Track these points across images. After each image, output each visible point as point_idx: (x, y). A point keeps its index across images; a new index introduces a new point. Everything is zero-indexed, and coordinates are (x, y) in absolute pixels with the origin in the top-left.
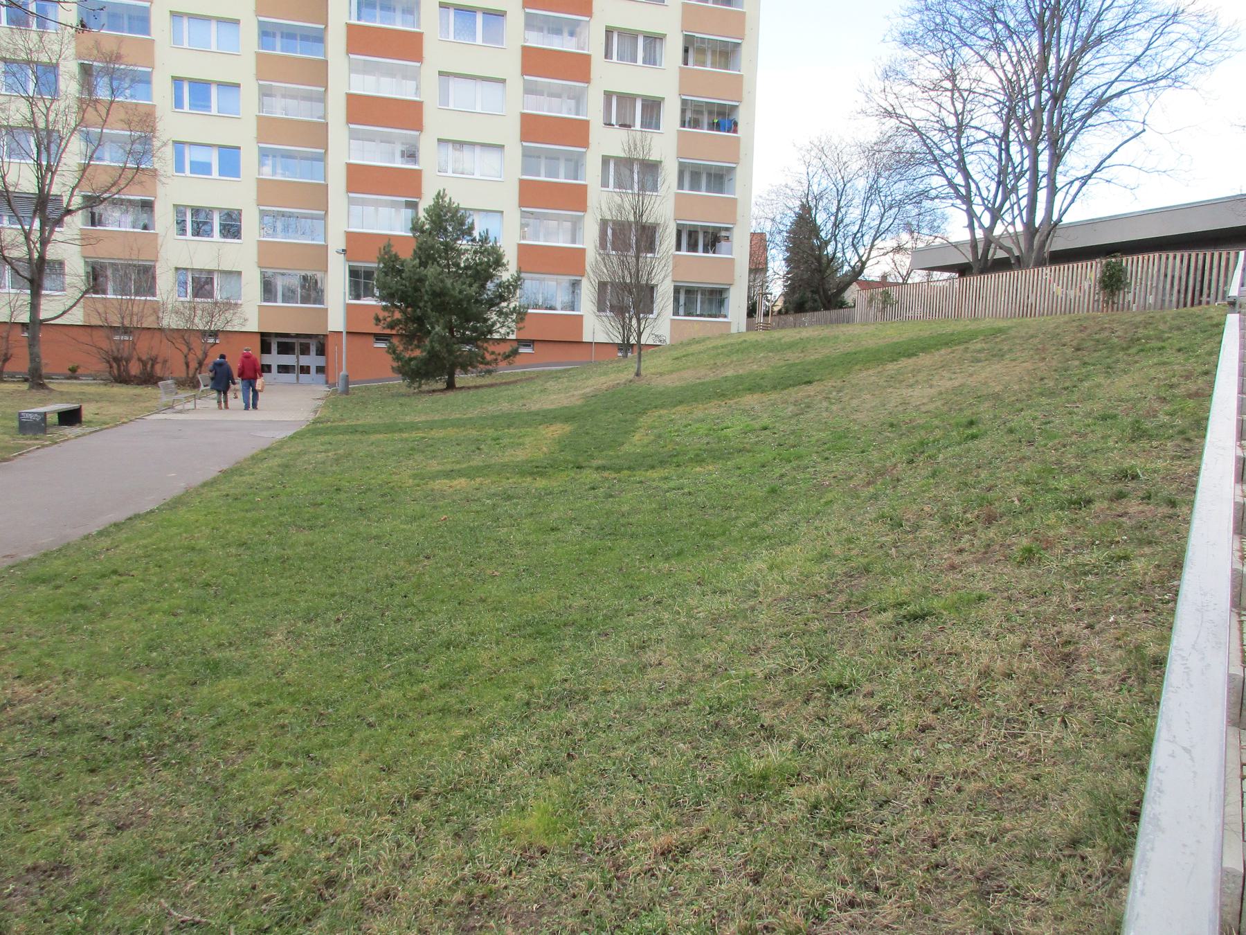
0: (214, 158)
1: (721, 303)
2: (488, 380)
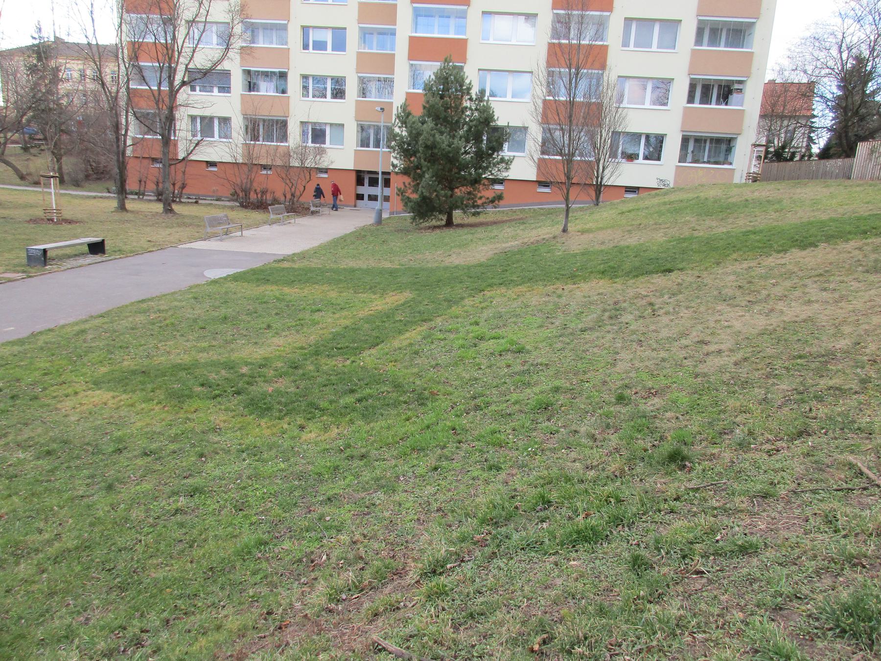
0: (328, 37)
1: (729, 150)
2: (473, 220)
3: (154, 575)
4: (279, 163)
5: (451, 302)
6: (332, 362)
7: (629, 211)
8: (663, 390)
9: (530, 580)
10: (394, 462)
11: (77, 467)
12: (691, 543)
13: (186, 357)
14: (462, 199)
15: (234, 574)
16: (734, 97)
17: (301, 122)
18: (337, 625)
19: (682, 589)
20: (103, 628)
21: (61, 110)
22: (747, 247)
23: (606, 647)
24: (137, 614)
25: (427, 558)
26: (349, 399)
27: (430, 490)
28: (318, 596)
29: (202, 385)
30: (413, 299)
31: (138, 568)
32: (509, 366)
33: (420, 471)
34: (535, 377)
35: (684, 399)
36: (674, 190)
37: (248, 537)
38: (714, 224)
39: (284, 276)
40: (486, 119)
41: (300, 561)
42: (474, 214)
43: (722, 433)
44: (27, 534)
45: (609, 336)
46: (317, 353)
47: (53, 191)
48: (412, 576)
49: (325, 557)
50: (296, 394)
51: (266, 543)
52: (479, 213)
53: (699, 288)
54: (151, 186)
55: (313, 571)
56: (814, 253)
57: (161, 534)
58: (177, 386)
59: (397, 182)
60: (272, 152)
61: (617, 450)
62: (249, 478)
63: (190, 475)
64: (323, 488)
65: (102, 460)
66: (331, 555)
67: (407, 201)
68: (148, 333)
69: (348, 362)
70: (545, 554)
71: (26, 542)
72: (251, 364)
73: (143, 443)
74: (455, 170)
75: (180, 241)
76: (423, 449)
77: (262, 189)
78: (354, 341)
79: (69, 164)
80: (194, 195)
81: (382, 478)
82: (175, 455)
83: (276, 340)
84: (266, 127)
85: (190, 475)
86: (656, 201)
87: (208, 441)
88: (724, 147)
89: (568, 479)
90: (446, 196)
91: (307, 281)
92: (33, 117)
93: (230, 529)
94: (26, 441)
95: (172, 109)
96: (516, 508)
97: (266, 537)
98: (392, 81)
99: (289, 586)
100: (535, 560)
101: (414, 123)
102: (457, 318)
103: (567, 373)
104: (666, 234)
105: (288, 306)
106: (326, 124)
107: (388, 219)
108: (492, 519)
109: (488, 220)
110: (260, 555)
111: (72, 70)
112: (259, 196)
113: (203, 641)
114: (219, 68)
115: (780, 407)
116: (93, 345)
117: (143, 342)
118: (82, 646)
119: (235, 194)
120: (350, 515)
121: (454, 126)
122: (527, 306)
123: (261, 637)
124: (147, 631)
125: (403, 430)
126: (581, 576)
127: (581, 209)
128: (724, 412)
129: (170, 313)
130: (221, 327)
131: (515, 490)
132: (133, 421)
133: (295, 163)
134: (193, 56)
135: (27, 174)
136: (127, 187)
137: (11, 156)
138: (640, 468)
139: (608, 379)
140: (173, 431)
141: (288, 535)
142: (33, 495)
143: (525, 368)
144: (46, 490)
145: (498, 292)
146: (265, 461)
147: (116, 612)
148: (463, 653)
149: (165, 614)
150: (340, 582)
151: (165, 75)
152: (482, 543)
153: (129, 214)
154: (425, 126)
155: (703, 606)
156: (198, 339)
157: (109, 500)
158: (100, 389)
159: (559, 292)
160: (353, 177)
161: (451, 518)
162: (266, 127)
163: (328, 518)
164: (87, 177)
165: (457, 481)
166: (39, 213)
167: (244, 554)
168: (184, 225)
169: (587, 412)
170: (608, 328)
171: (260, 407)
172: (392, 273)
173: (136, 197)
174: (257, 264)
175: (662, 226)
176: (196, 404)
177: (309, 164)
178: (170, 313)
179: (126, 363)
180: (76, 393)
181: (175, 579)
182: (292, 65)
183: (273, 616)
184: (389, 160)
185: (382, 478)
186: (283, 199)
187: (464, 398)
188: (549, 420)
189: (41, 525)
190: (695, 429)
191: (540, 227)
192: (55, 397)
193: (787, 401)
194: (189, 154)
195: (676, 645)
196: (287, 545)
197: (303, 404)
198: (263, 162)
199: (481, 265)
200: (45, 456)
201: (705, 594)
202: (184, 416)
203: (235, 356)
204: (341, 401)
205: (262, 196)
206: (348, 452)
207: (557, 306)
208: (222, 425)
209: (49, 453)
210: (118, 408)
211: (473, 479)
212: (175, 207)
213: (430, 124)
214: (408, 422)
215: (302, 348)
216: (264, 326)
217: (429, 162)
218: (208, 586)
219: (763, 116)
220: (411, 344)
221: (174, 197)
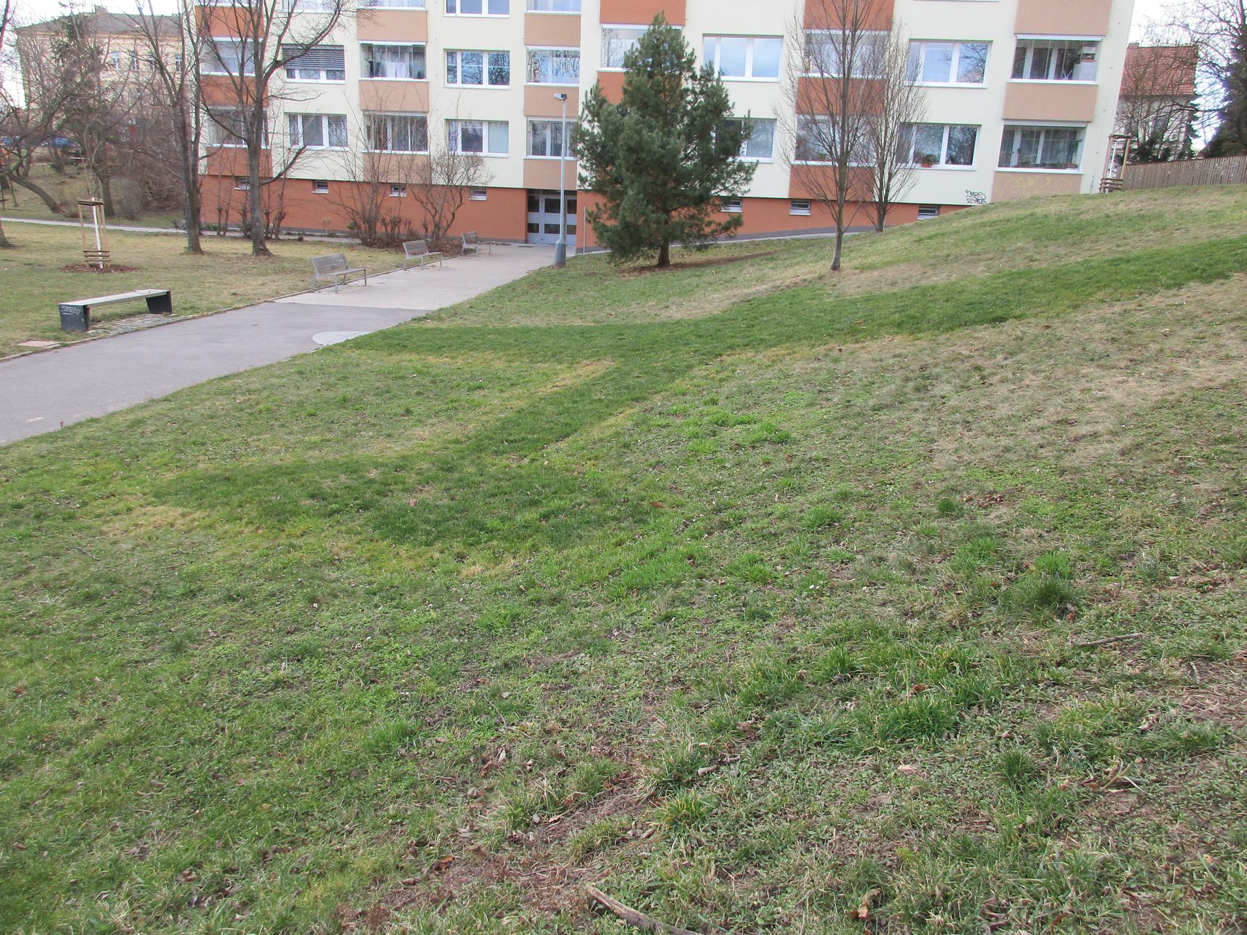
1: (1073, 147)
2: (697, 257)
3: (244, 782)
4: (416, 179)
5: (673, 373)
6: (502, 462)
7: (930, 238)
8: (1011, 494)
9: (837, 796)
10: (601, 608)
11: (131, 618)
12: (1099, 735)
13: (288, 456)
14: (682, 225)
15: (366, 781)
16: (1084, 66)
17: (447, 120)
18: (527, 866)
19: (1095, 813)
20: (167, 864)
21: (105, 110)
22: (1120, 281)
23: (983, 914)
24: (218, 844)
25: (666, 759)
26: (531, 515)
27: (660, 650)
28: (496, 818)
29: (313, 496)
30: (617, 370)
31: (219, 771)
32: (767, 463)
33: (644, 621)
34: (809, 479)
35: (1048, 509)
36: (994, 206)
37: (386, 725)
38: (1062, 251)
39: (427, 340)
40: (716, 102)
41: (466, 761)
42: (699, 249)
43: (1116, 558)
44: (54, 719)
45: (918, 417)
46: (479, 449)
47: (96, 226)
48: (643, 788)
49: (503, 755)
50: (450, 509)
51: (412, 734)
52: (706, 247)
53: (1050, 343)
54: (235, 217)
55: (486, 776)
56: (1225, 287)
57: (253, 719)
58: (273, 500)
59: (586, 204)
60: (406, 164)
61: (950, 587)
62: (385, 633)
63: (296, 629)
64: (495, 648)
65: (166, 608)
66: (513, 752)
67: (601, 231)
68: (234, 423)
69: (526, 461)
70: (856, 753)
71: (52, 730)
72: (382, 465)
73: (226, 581)
74: (671, 185)
75: (278, 294)
76: (646, 589)
77: (395, 218)
78: (533, 431)
79: (120, 187)
80: (297, 229)
81: (585, 633)
82: (274, 600)
83: (418, 431)
84: (396, 128)
85: (296, 629)
86: (968, 222)
87: (322, 579)
88: (1063, 145)
89: (879, 633)
90: (658, 222)
91: (461, 346)
92: (67, 121)
93: (357, 711)
94: (55, 580)
95: (261, 102)
96: (801, 678)
97: (411, 723)
98: (576, 55)
99: (450, 801)
100: (841, 762)
101: (610, 114)
102: (684, 394)
103: (857, 471)
104: (989, 268)
105: (434, 382)
106: (481, 122)
107: (576, 257)
108: (762, 696)
109: (719, 256)
110: (403, 751)
111: (118, 50)
112: (389, 228)
113: (319, 889)
114: (326, 41)
115: (1204, 517)
116: (154, 440)
117: (226, 436)
118: (135, 893)
119: (355, 225)
120: (539, 689)
121: (668, 123)
122: (787, 376)
123: (409, 884)
124: (234, 871)
125: (614, 559)
126: (923, 790)
127: (857, 238)
128: (1115, 525)
129: (265, 394)
130: (338, 414)
131: (794, 650)
132: (211, 549)
133: (439, 180)
134: (288, 23)
135: (62, 204)
136: (202, 220)
137: (38, 178)
138: (991, 614)
139: (923, 480)
140: (270, 564)
141: (445, 720)
142: (64, 659)
143: (793, 465)
144: (85, 652)
145: (743, 356)
146: (407, 609)
147: (187, 838)
148: (739, 919)
149: (262, 845)
150: (530, 796)
151: (248, 54)
152: (751, 735)
153: (205, 257)
154: (626, 118)
155: (1139, 843)
156: (305, 431)
157: (177, 667)
158: (164, 503)
159: (835, 354)
160: (523, 200)
161: (696, 694)
162: (396, 128)
163: (505, 695)
164: (146, 207)
165: (703, 636)
166: (78, 256)
167: (381, 750)
168: (284, 271)
169: (896, 530)
170: (916, 404)
171: (398, 528)
172: (584, 333)
173: (215, 233)
174: (388, 324)
175: (981, 257)
176: (303, 524)
177: (458, 180)
178: (265, 394)
179: (201, 465)
180: (129, 510)
181: (276, 788)
182: (431, 38)
183: (427, 848)
184: (573, 172)
185: (585, 633)
186: (422, 232)
187: (703, 511)
188: (837, 542)
189: (76, 704)
190: (1074, 552)
191: (797, 264)
192: (98, 516)
193: (1215, 508)
194: (286, 169)
195: (1104, 910)
196: (443, 736)
197: (462, 522)
198: (393, 179)
199: (714, 319)
200: (83, 602)
201: (1138, 821)
202: (286, 542)
203: (360, 454)
204: (518, 517)
205: (393, 229)
206: (532, 594)
207: (833, 375)
208: (342, 555)
209: (89, 597)
210: (189, 531)
211: (726, 633)
212: (270, 247)
213: (633, 114)
214: (619, 549)
215: (457, 442)
216: (401, 411)
217: (633, 172)
218: (325, 800)
219: (1125, 97)
220: (618, 434)
221: (268, 232)
